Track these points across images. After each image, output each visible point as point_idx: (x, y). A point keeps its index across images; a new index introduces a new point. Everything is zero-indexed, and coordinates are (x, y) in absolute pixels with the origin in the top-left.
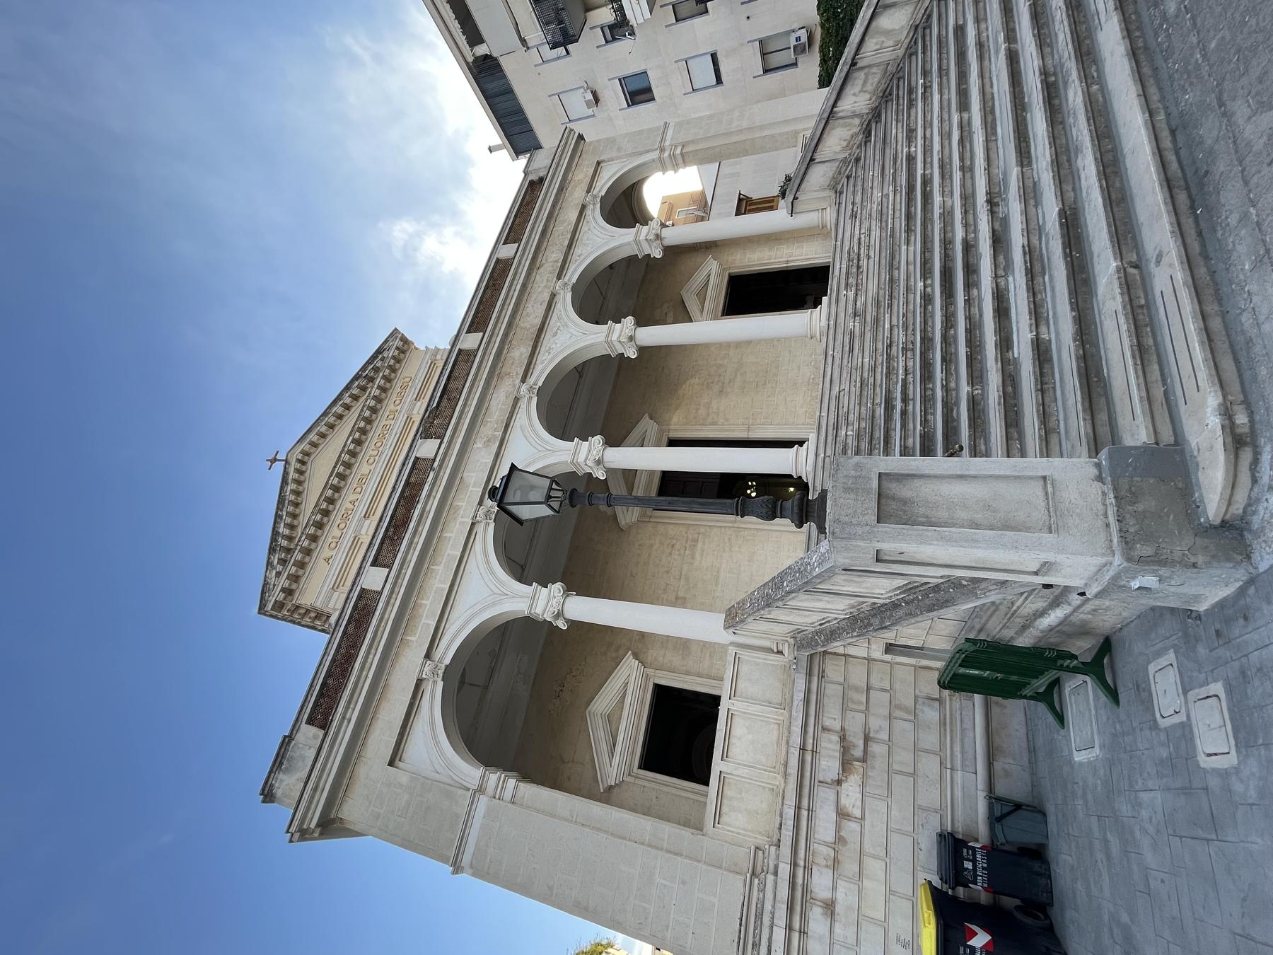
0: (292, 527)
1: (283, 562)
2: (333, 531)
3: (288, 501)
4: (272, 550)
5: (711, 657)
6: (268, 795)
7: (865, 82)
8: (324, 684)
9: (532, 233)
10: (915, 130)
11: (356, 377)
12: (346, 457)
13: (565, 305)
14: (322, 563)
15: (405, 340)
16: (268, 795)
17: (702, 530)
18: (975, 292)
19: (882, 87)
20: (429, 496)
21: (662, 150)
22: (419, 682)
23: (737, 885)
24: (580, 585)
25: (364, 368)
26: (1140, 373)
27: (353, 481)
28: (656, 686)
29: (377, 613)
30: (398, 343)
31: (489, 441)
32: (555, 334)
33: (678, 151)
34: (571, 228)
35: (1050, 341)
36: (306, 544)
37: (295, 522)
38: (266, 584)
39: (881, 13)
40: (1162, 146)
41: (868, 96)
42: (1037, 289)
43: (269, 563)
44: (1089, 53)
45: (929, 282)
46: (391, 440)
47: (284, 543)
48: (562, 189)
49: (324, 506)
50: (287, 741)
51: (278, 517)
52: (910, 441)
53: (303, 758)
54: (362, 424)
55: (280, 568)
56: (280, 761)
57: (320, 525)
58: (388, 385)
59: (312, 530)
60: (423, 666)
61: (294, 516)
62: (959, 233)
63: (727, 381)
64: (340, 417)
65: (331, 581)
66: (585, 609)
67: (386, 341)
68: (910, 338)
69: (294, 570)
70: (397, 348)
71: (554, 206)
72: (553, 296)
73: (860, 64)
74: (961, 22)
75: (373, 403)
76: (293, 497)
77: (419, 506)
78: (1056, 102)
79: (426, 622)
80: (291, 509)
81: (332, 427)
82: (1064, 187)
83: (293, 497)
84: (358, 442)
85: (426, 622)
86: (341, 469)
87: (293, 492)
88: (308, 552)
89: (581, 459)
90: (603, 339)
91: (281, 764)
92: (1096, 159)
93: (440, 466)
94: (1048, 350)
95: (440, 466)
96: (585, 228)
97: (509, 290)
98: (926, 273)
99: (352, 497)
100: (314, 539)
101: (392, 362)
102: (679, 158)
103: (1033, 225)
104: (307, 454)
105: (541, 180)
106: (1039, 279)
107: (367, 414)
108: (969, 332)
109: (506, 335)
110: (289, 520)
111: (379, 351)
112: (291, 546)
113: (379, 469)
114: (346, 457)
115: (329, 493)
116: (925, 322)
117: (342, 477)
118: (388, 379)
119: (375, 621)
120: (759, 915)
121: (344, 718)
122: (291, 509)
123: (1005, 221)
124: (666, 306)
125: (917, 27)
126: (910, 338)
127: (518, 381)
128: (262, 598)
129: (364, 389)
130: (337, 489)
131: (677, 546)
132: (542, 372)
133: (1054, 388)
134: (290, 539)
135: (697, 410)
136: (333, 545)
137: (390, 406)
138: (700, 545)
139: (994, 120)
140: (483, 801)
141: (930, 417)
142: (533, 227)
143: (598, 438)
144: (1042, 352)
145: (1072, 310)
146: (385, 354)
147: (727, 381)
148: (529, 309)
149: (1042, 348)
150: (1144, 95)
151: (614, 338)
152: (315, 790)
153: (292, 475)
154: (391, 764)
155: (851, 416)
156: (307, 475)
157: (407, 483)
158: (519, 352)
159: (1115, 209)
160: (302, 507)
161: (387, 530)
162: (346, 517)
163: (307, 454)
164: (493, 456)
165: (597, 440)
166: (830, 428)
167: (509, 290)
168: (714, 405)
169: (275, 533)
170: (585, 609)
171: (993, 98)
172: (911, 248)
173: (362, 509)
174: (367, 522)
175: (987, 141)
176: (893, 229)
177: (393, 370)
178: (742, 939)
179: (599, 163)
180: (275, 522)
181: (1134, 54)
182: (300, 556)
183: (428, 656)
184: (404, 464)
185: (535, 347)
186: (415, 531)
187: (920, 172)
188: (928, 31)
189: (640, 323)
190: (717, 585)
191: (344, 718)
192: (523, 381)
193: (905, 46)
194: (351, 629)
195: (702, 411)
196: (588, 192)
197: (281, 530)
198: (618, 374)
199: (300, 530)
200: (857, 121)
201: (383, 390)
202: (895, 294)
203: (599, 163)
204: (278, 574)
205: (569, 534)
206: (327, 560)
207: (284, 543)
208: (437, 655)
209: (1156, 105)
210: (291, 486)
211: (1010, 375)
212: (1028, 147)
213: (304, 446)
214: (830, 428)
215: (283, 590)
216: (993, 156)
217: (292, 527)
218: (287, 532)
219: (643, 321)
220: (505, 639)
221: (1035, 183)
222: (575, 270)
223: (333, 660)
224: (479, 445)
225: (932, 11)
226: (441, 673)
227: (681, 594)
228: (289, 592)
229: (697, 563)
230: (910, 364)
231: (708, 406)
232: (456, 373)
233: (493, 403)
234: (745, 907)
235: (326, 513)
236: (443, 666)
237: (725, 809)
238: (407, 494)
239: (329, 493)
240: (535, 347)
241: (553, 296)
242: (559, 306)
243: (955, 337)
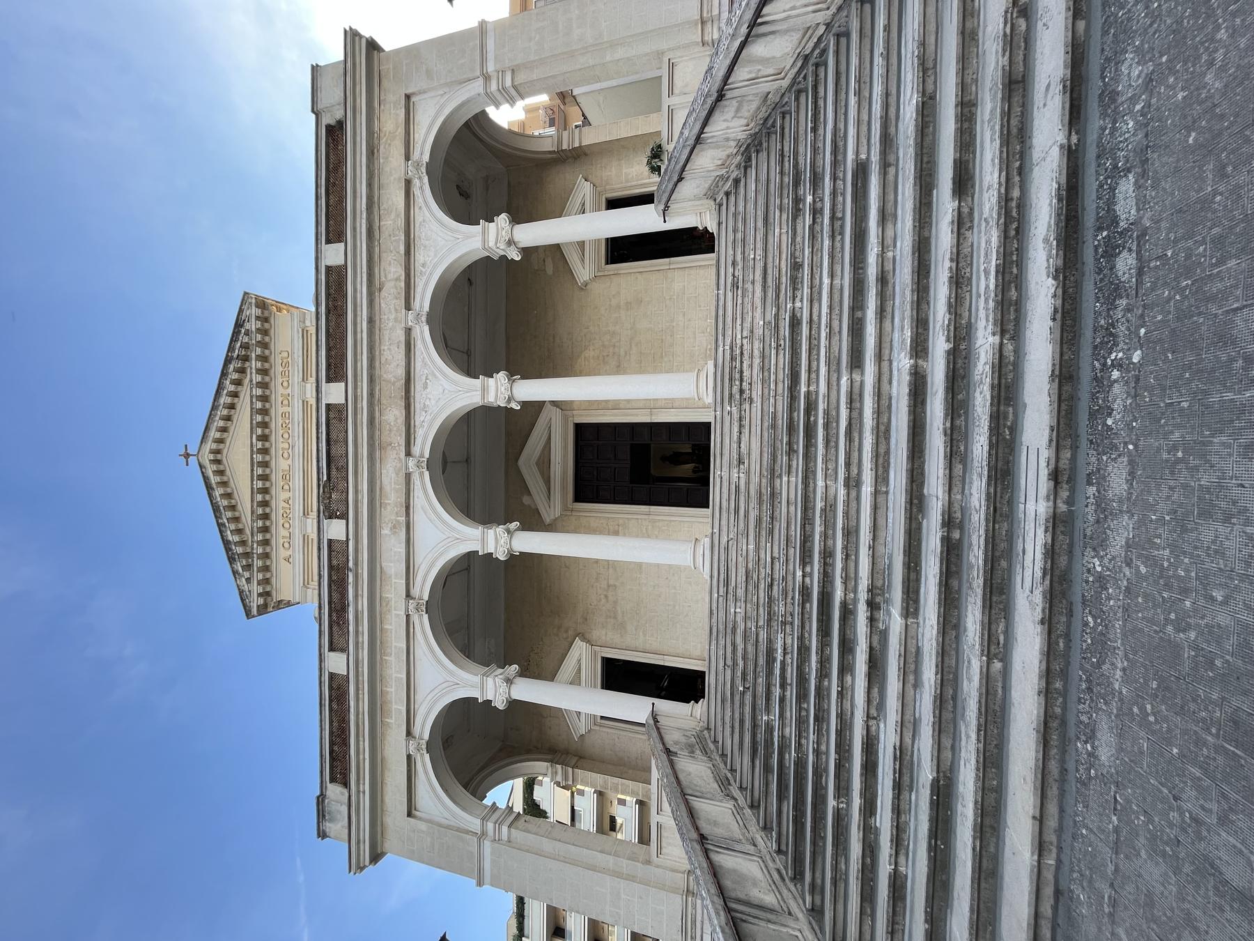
0: (239, 531)
1: (248, 567)
2: (279, 534)
3: (222, 507)
4: (231, 560)
5: (645, 635)
6: (322, 834)
7: (738, 110)
8: (331, 752)
9: (356, 222)
10: (802, 265)
11: (228, 361)
12: (259, 458)
13: (426, 347)
14: (283, 563)
15: (262, 304)
16: (322, 834)
17: (621, 522)
18: (849, 678)
19: (762, 115)
20: (356, 596)
21: (487, 78)
22: (409, 757)
23: (677, 901)
24: (521, 368)
25: (231, 348)
27: (276, 478)
28: (603, 658)
29: (352, 710)
30: (254, 311)
31: (394, 527)
32: (425, 387)
33: (508, 83)
34: (401, 222)
35: (906, 876)
36: (260, 550)
37: (240, 526)
38: (241, 592)
39: (753, 42)
40: (1042, 909)
41: (744, 122)
42: (902, 807)
43: (235, 573)
44: (1002, 592)
45: (808, 569)
46: (297, 430)
47: (240, 550)
48: (371, 152)
49: (260, 511)
50: (321, 799)
51: (221, 526)
52: (787, 730)
53: (340, 812)
54: (259, 418)
55: (247, 574)
56: (321, 814)
57: (265, 530)
58: (267, 365)
59: (260, 537)
60: (407, 746)
61: (236, 519)
62: (838, 594)
63: (622, 353)
64: (232, 407)
65: (299, 580)
66: (535, 234)
67: (241, 311)
68: (790, 609)
69: (260, 576)
70: (258, 318)
71: (370, 185)
72: (408, 331)
73: (729, 95)
74: (863, 156)
75: (259, 392)
76: (225, 503)
77: (351, 609)
78: (955, 583)
79: (397, 707)
80: (229, 514)
81: (228, 418)
82: (943, 740)
83: (225, 503)
84: (264, 438)
85: (397, 707)
86: (260, 484)
87: (223, 496)
88: (266, 556)
89: (492, 244)
91: (324, 816)
92: (975, 825)
93: (356, 564)
94: (904, 886)
95: (356, 564)
96: (419, 219)
97: (355, 333)
98: (806, 558)
99: (284, 495)
100: (266, 543)
101: (259, 337)
102: (514, 93)
103: (908, 717)
104: (218, 452)
105: (341, 124)
106: (905, 795)
107: (259, 405)
108: (839, 733)
109: (371, 394)
110: (233, 527)
111: (239, 325)
112: (248, 551)
113: (298, 465)
114: (259, 458)
115: (259, 497)
116: (803, 627)
117: (264, 478)
118: (264, 359)
119: (352, 717)
120: (694, 922)
121: (358, 792)
122: (229, 514)
123: (884, 635)
125: (806, 58)
126: (790, 609)
127: (403, 454)
128: (245, 606)
129: (242, 371)
130: (265, 491)
132: (425, 438)
133: (903, 931)
134: (243, 543)
136: (286, 545)
137: (279, 391)
139: (888, 452)
140: (487, 844)
141: (803, 741)
142: (354, 229)
143: (504, 216)
145: (926, 921)
146: (247, 326)
147: (622, 353)
148: (387, 355)
149: (898, 883)
150: (1040, 819)
151: (492, 244)
152: (358, 842)
153: (214, 480)
154: (409, 815)
155: (739, 591)
156: (228, 472)
157: (331, 567)
158: (393, 416)
159: (983, 885)
160: (239, 507)
161: (330, 616)
162: (286, 516)
163: (218, 452)
164: (404, 545)
165: (503, 219)
166: (722, 551)
167: (355, 333)
169: (226, 543)
170: (535, 234)
171: (890, 398)
172: (793, 479)
173: (298, 508)
174: (309, 591)
175: (876, 493)
176: (775, 413)
177: (265, 346)
178: (684, 930)
179: (408, 97)
180: (221, 532)
181: (1048, 675)
182: (260, 563)
183: (409, 733)
184: (319, 549)
185: (408, 407)
186: (357, 632)
187: (803, 389)
188: (822, 70)
189: (516, 219)
191: (358, 792)
192: (408, 454)
193: (790, 76)
194: (335, 706)
196: (407, 158)
197: (230, 538)
198: (508, 346)
199: (248, 532)
200: (733, 144)
201: (264, 372)
202: (777, 513)
203: (408, 97)
204: (248, 580)
205: (500, 316)
206: (287, 560)
207: (240, 550)
208: (416, 730)
209: (1051, 837)
210: (218, 492)
211: (870, 846)
212: (918, 580)
213: (210, 445)
214: (722, 551)
215: (260, 595)
216: (881, 522)
217: (239, 531)
218: (236, 538)
219: (518, 217)
220: (466, 569)
221: (918, 648)
222: (426, 284)
223: (331, 733)
224: (386, 531)
225: (827, 45)
226: (424, 747)
227: (611, 582)
228: (266, 594)
230: (789, 641)
232: (333, 436)
233: (385, 481)
234: (684, 917)
235: (266, 517)
236: (424, 742)
237: (664, 844)
238: (334, 578)
239: (259, 497)
240: (408, 407)
241: (408, 331)
242: (419, 200)
243: (829, 689)
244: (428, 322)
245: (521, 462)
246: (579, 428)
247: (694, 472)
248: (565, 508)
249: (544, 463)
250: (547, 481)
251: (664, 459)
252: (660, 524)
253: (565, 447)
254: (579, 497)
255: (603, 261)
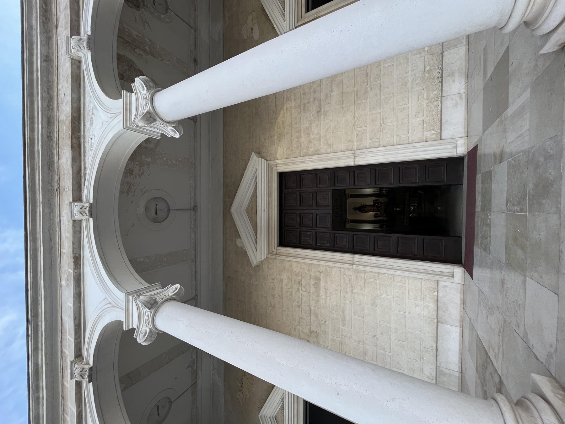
13: (93, 90)
17: (322, 269)
26: (436, 273)
63: (323, 97)
90: (120, 126)
124: (250, 17)
131: (303, 283)
135: (298, 137)
138: (322, 284)
144: (424, 151)
147: (323, 97)
168: (314, 130)
190: (344, 324)
195: (304, 139)
220: (118, 338)
227: (313, 328)
229: (322, 302)
231: (308, 132)
244: (89, 47)
245: (233, 210)
246: (283, 177)
247: (375, 217)
248: (270, 252)
249: (252, 211)
250: (255, 227)
251: (356, 209)
252: (362, 275)
253: (270, 195)
254: (283, 242)
255: (303, 10)
